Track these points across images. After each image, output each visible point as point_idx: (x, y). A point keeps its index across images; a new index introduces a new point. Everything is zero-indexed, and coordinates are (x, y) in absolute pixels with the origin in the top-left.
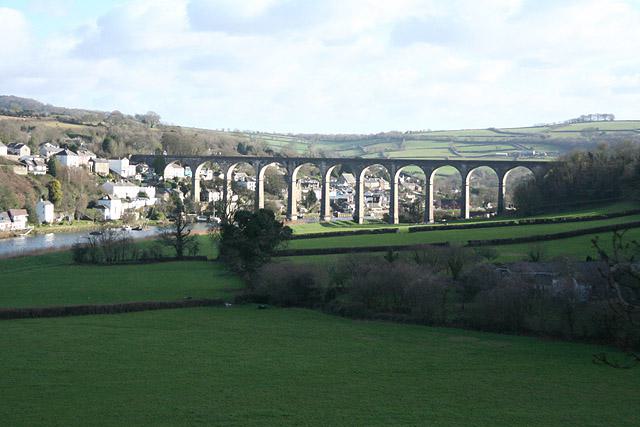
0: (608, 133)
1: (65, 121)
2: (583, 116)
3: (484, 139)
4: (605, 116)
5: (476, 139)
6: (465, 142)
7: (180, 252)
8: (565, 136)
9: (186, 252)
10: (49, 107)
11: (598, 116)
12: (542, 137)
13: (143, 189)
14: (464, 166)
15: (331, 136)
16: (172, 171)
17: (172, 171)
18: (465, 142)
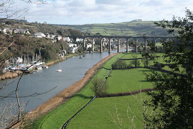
0: (143, 24)
1: (27, 25)
2: (134, 20)
3: (112, 26)
4: (139, 20)
5: (110, 26)
6: (107, 27)
7: (136, 66)
8: (133, 25)
9: (137, 66)
10: (36, 24)
11: (138, 20)
12: (127, 25)
13: (74, 45)
14: (154, 38)
15: (74, 25)
16: (78, 40)
17: (78, 40)
18: (107, 27)
